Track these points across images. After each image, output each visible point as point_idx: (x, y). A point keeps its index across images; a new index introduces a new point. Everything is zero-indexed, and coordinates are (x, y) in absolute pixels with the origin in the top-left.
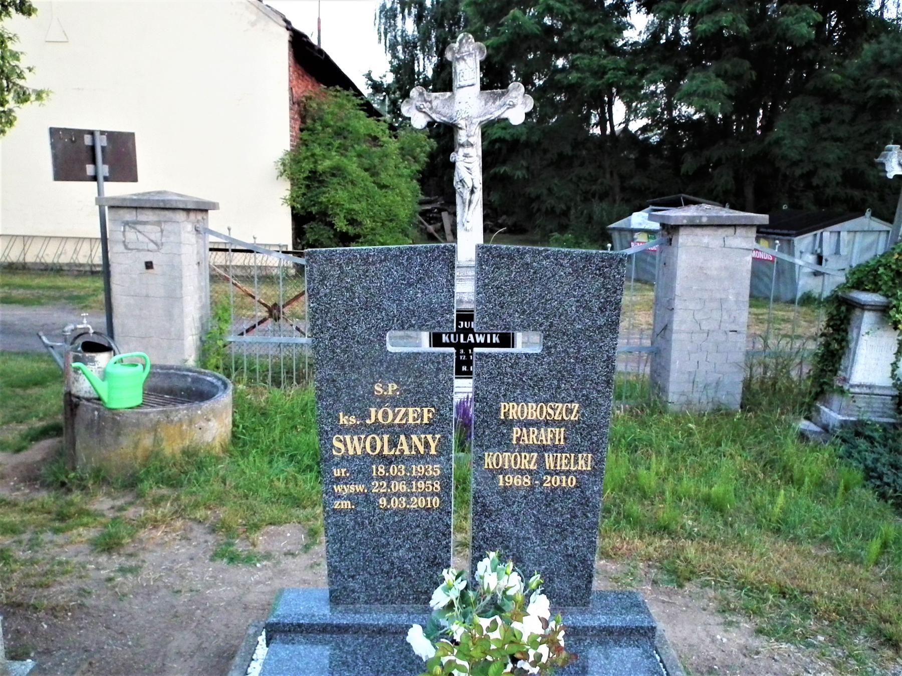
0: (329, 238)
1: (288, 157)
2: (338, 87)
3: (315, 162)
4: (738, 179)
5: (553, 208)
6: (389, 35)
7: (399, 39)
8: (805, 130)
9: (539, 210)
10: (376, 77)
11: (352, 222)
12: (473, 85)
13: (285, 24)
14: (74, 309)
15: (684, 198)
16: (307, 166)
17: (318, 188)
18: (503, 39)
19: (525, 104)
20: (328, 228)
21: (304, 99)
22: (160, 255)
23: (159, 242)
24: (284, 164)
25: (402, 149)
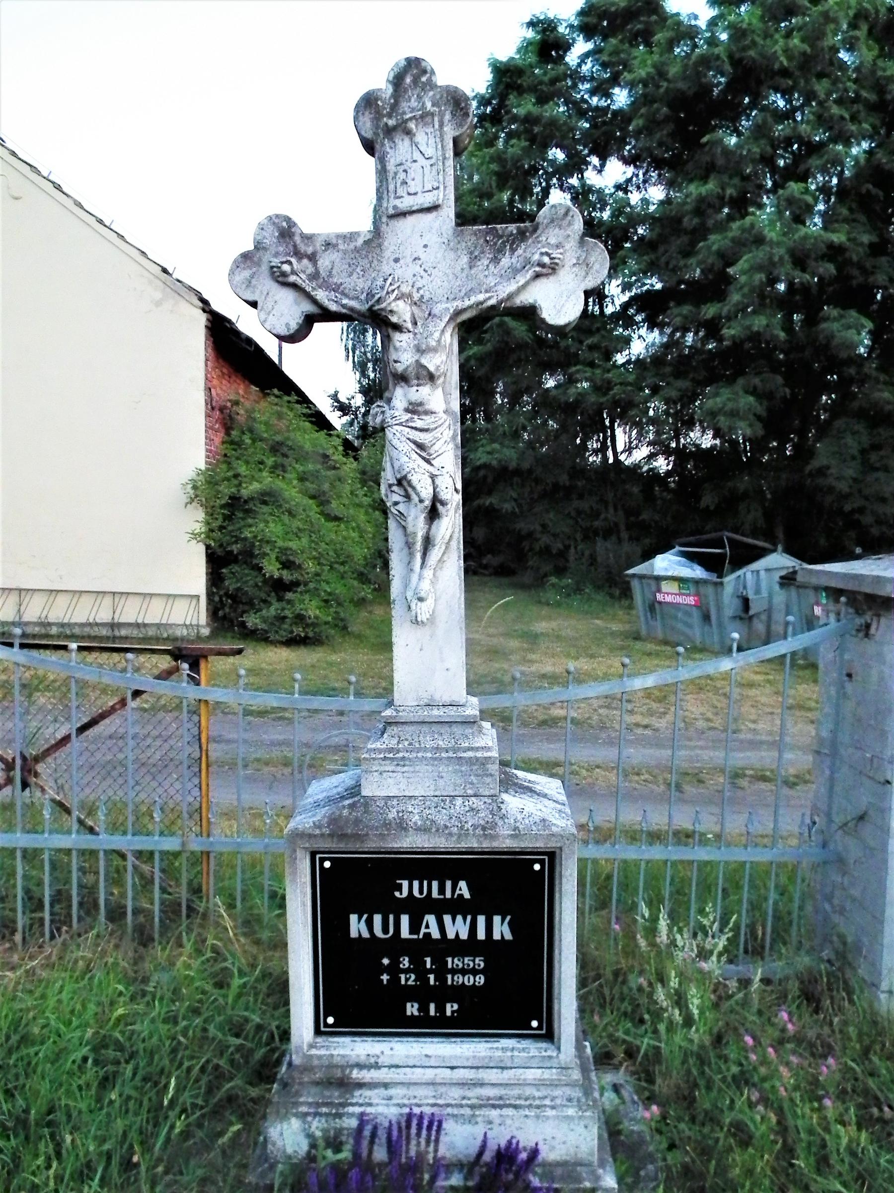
0: (257, 585)
1: (201, 477)
2: (276, 391)
4: (768, 516)
6: (357, 352)
7: (369, 355)
8: (853, 458)
9: (531, 549)
10: (343, 398)
11: (287, 565)
12: (433, 208)
13: (200, 304)
15: (728, 538)
16: (227, 490)
17: (243, 519)
18: (489, 347)
19: (585, 264)
20: (254, 573)
21: (229, 404)
24: (195, 488)
25: (363, 473)
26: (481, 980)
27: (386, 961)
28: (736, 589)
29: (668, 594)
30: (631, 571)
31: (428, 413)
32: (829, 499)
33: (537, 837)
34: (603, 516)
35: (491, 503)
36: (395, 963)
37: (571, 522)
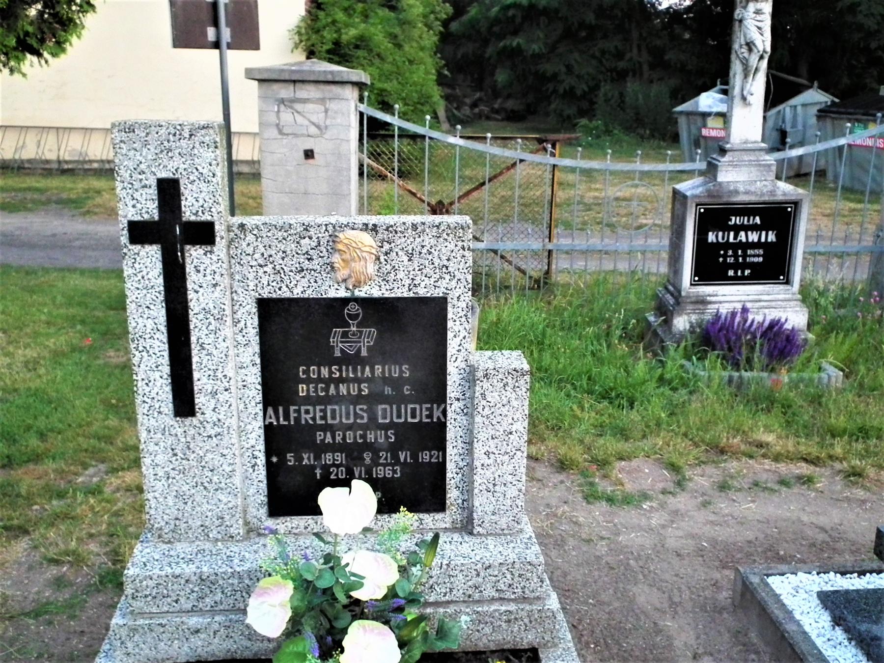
3: (338, 31)
5: (572, 88)
9: (555, 91)
14: (73, 216)
22: (323, 141)
23: (322, 124)
24: (299, 33)
26: (761, 259)
27: (722, 252)
28: (776, 123)
29: (713, 129)
30: (679, 108)
31: (762, 13)
32: (856, 36)
33: (792, 195)
34: (628, 56)
35: (518, 44)
36: (726, 252)
37: (594, 62)
